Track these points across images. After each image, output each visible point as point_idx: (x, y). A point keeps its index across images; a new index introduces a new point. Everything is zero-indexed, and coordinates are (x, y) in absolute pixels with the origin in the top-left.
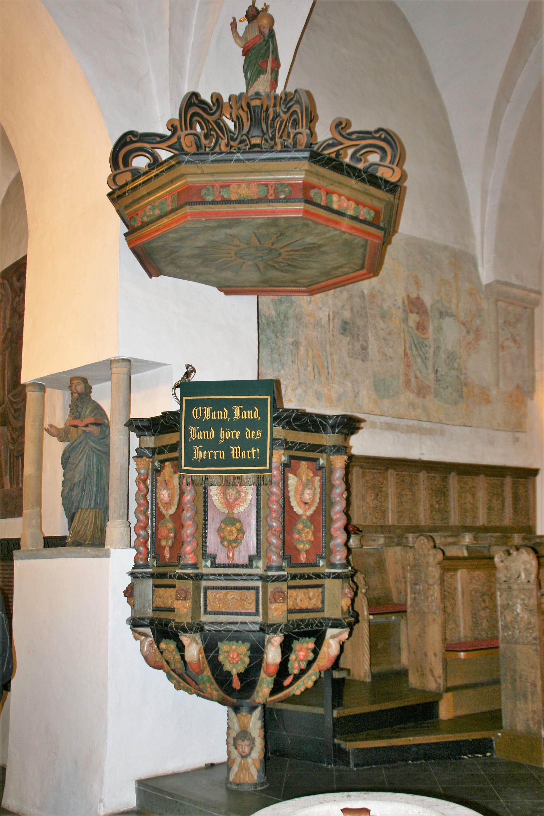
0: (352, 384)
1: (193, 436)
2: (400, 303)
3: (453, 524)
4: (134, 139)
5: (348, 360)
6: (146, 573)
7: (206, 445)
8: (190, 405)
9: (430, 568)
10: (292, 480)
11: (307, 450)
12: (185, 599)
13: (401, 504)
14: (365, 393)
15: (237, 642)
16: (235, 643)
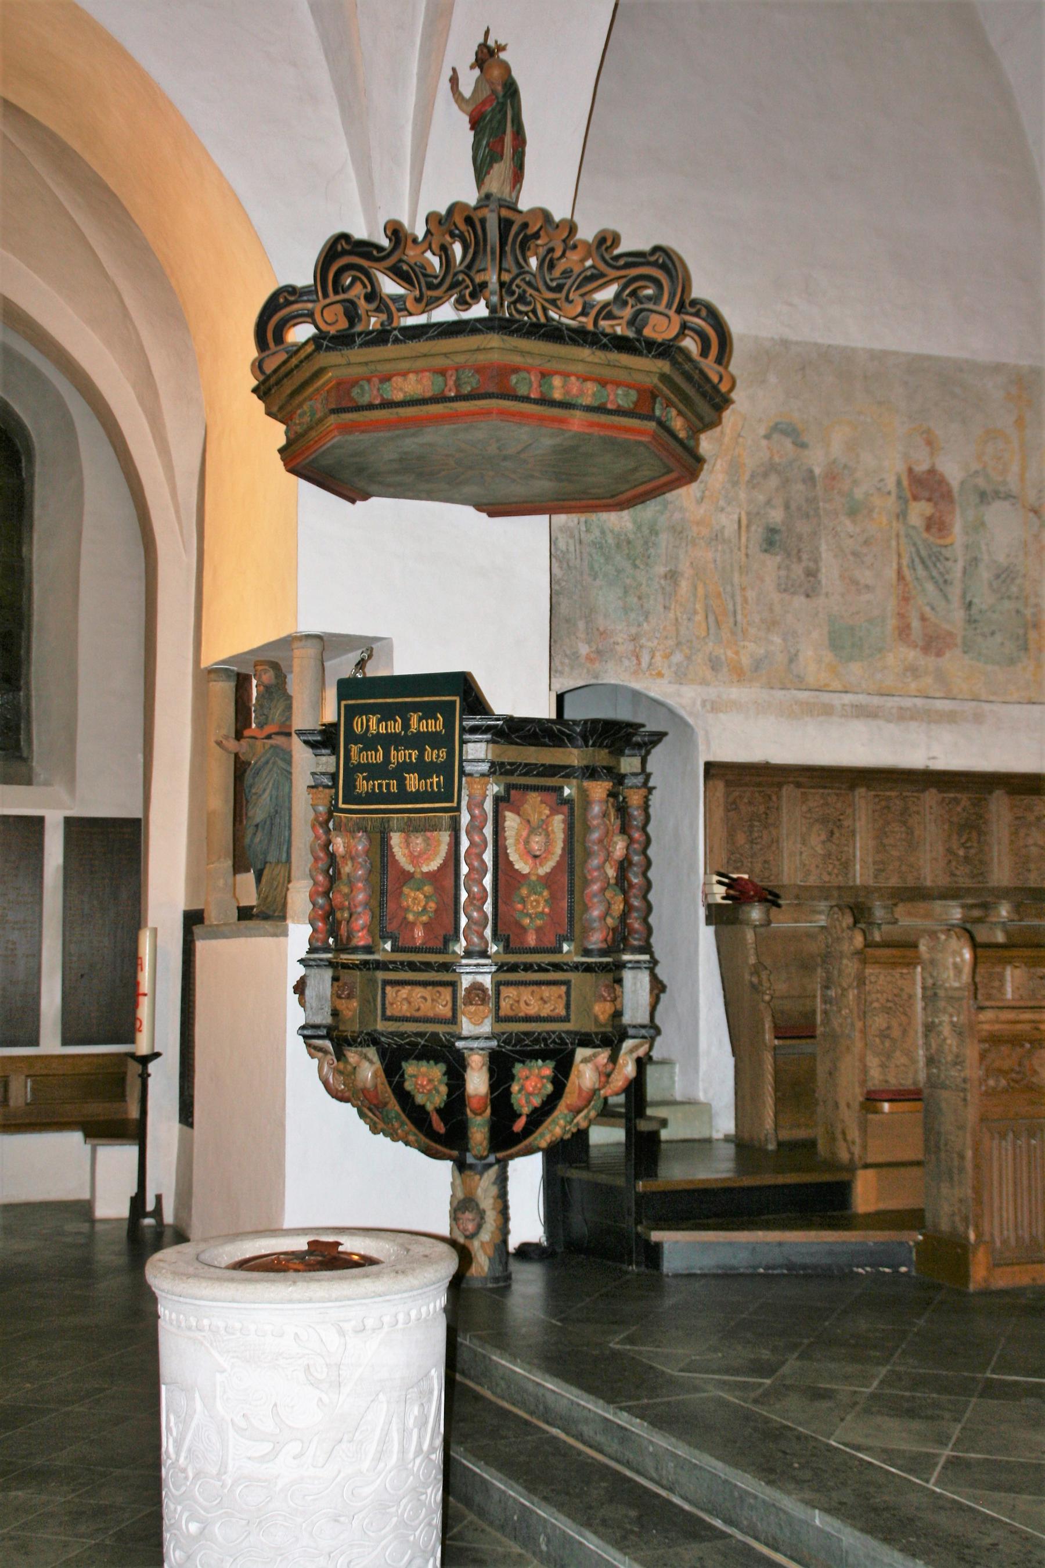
0: (784, 640)
1: (354, 760)
2: (891, 484)
3: (996, 884)
4: (292, 298)
5: (775, 597)
6: (321, 960)
7: (374, 771)
8: (351, 713)
9: (845, 961)
10: (511, 821)
11: (538, 775)
12: (349, 997)
13: (881, 847)
14: (810, 653)
15: (428, 1062)
16: (424, 1063)
